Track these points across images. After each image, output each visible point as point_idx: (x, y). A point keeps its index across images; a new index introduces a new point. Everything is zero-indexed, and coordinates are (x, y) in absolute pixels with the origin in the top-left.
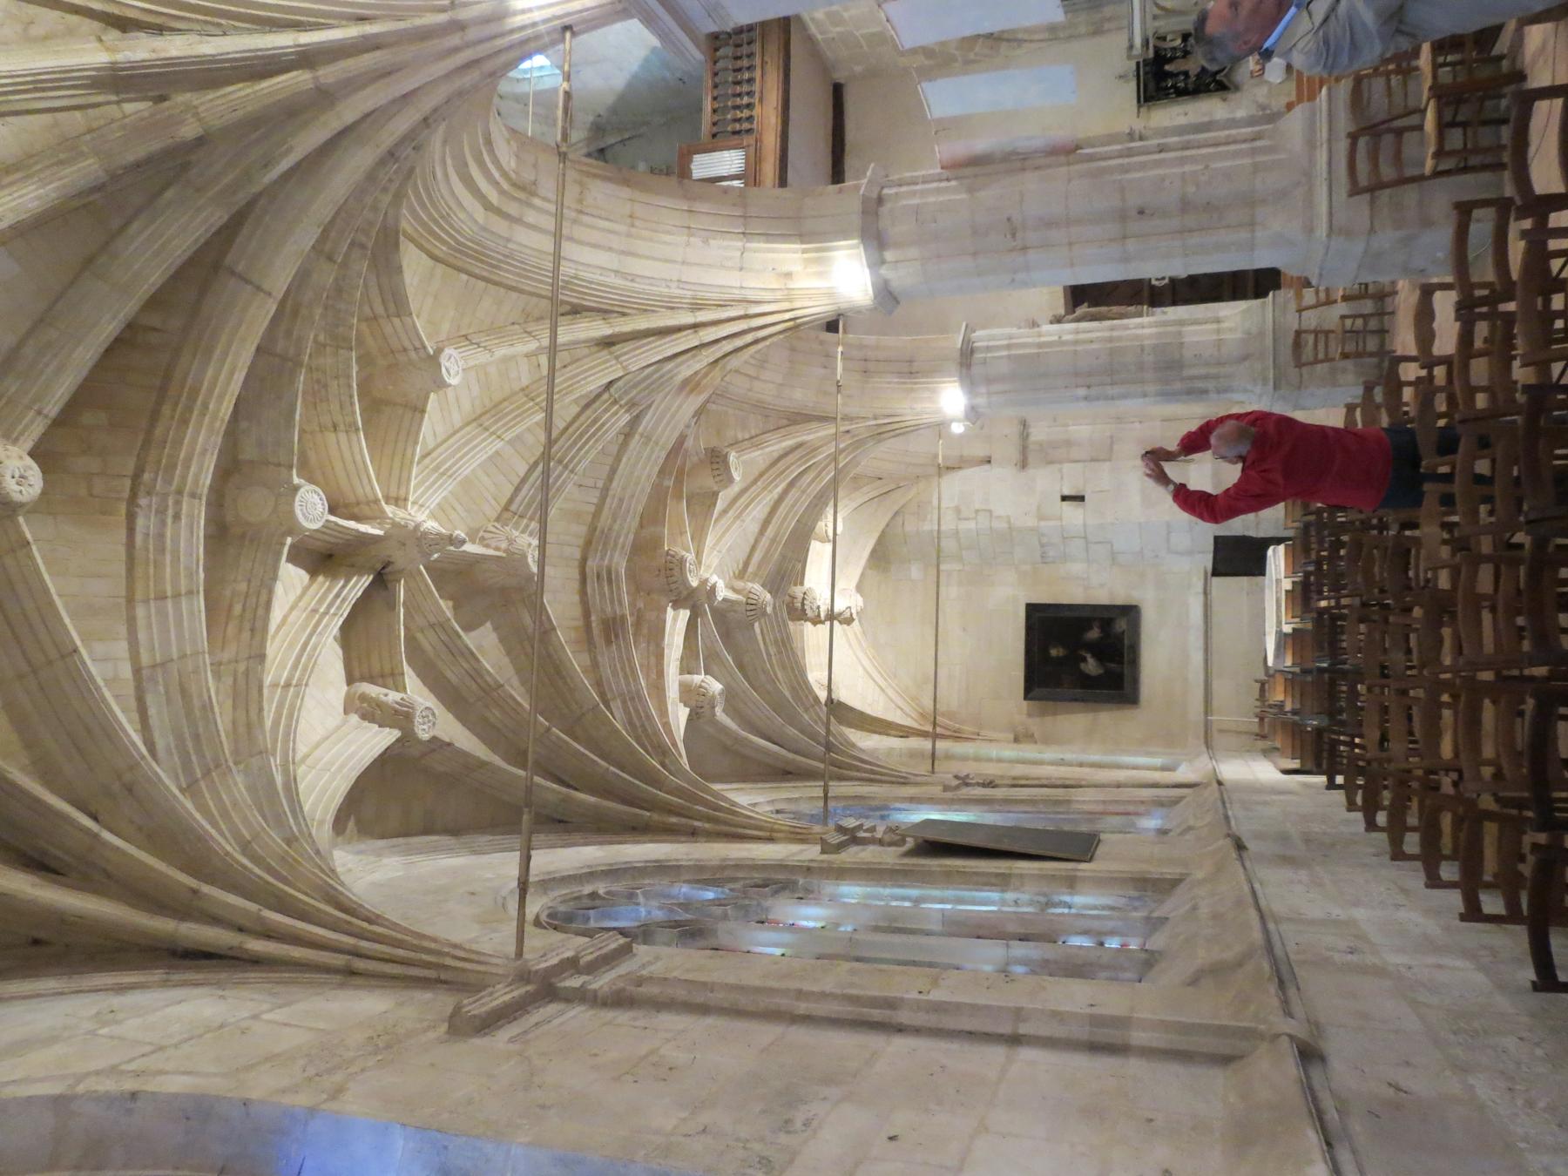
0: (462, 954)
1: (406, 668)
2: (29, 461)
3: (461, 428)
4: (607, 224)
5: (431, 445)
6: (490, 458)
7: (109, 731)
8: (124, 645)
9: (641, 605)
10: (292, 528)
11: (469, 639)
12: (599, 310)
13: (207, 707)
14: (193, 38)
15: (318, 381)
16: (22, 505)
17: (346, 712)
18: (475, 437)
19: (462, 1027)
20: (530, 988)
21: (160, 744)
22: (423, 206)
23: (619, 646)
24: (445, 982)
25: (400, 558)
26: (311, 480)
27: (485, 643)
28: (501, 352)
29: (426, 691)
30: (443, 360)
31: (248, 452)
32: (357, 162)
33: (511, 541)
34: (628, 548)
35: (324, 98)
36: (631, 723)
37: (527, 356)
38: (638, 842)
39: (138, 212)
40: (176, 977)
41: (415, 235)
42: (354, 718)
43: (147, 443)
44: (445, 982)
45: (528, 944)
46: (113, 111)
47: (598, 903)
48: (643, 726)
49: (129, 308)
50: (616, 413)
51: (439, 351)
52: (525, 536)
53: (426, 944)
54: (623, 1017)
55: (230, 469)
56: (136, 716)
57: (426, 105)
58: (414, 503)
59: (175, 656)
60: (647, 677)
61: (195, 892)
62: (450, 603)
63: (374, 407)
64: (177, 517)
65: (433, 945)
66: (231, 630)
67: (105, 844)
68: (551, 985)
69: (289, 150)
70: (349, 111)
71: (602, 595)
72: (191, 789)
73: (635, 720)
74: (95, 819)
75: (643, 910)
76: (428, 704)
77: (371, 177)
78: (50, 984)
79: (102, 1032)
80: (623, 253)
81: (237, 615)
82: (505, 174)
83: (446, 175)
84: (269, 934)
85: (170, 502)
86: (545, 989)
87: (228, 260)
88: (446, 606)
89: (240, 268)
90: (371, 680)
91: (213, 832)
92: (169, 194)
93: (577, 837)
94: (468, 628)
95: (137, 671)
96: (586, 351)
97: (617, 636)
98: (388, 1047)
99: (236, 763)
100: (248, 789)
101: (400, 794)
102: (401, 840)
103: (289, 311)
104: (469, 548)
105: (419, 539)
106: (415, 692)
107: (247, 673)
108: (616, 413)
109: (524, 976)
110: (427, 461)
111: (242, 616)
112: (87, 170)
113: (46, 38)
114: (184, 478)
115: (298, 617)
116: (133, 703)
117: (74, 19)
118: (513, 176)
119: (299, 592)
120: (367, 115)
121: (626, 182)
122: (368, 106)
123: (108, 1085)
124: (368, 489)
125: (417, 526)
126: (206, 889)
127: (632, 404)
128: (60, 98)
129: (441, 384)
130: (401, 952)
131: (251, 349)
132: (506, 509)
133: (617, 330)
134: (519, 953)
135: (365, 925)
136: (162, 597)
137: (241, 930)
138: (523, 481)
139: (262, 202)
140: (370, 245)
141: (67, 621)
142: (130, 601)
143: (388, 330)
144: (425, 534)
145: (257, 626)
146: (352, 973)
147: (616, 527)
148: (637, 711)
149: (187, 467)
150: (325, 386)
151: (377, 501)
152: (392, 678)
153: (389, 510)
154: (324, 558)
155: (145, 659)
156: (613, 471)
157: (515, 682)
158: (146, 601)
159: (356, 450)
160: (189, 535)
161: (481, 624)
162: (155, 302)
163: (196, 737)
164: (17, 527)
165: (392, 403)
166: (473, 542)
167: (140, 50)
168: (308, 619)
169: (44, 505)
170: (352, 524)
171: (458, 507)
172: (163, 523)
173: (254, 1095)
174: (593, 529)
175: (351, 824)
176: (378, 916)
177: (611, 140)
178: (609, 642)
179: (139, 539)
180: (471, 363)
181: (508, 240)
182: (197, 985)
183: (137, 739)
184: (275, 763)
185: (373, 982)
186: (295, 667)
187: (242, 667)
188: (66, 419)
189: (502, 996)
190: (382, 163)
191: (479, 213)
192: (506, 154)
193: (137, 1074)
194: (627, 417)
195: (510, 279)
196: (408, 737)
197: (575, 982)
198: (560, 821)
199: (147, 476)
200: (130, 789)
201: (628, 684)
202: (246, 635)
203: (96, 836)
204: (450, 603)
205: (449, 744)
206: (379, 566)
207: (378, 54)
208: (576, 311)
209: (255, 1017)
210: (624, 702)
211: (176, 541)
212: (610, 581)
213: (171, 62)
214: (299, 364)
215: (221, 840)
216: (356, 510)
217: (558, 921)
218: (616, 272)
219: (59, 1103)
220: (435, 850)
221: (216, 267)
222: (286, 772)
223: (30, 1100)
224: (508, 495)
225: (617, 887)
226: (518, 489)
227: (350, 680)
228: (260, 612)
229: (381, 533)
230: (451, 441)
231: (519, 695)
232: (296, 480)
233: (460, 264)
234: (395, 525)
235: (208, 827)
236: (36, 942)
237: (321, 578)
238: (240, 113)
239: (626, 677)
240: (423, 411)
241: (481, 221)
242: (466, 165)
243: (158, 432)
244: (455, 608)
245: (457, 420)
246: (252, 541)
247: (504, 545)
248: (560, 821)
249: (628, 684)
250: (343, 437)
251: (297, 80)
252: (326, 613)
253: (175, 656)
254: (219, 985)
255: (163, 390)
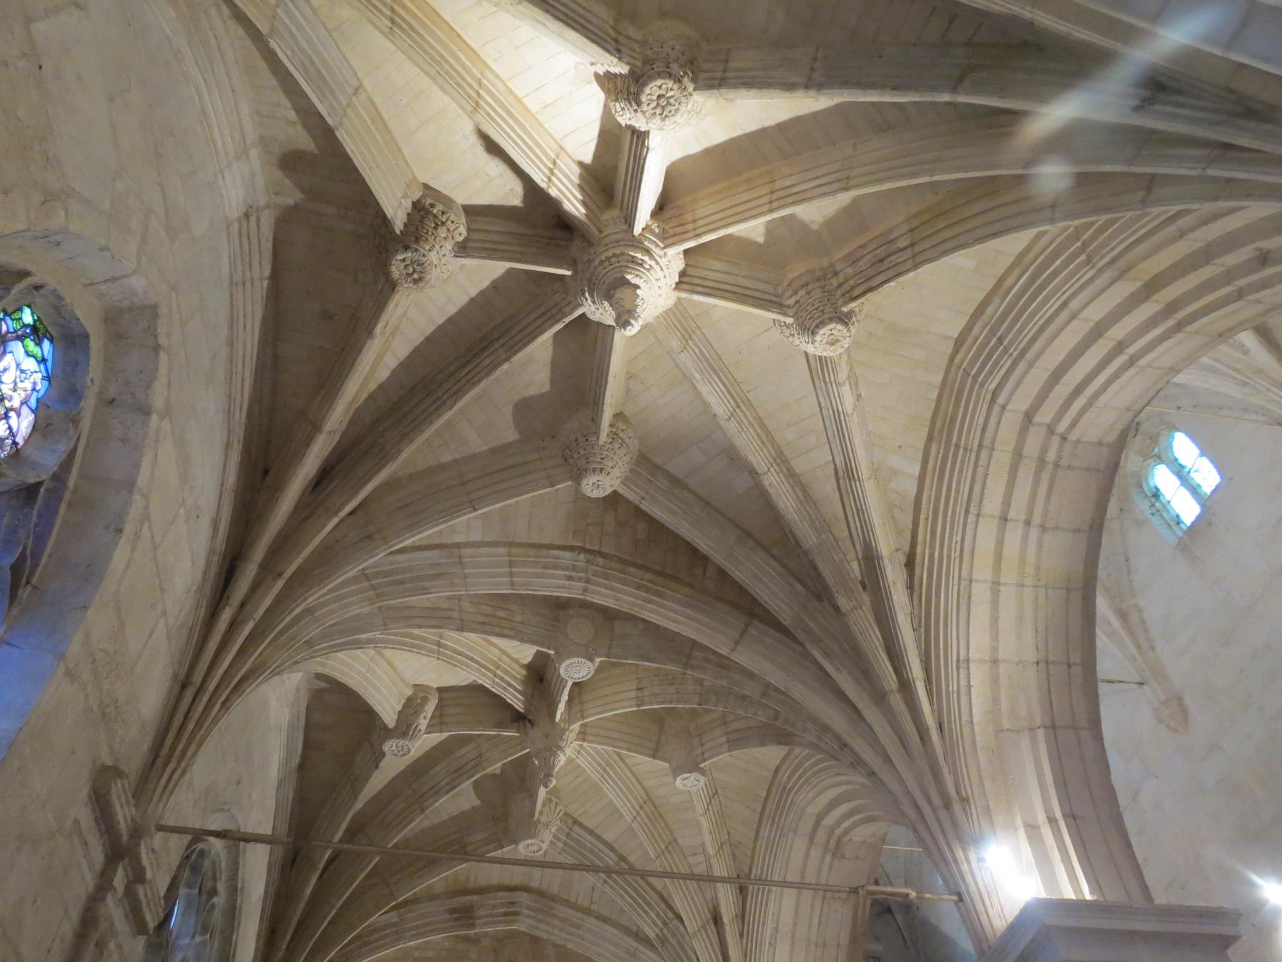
0: (176, 776)
1: (445, 735)
2: (609, 491)
3: (643, 787)
4: (816, 921)
5: (628, 761)
6: (618, 810)
7: (412, 527)
8: (478, 538)
9: (485, 942)
10: (561, 656)
11: (467, 785)
12: (744, 911)
13: (425, 591)
14: (908, 609)
15: (674, 679)
16: (579, 484)
17: (415, 686)
18: (635, 798)
19: (103, 777)
20: (125, 838)
21: (401, 557)
22: (813, 766)
23: (444, 921)
24: (154, 762)
25: (535, 733)
26: (599, 670)
27: (463, 799)
28: (704, 822)
29: (425, 749)
30: (694, 775)
31: (619, 627)
32: (838, 721)
33: (547, 825)
34: (537, 933)
35: (880, 698)
36: (373, 932)
37: (703, 845)
38: (259, 935)
39: (785, 566)
40: (215, 559)
41: (792, 756)
42: (409, 692)
43: (622, 561)
44: (154, 762)
45: (175, 837)
46: (851, 555)
47: (204, 897)
48: (369, 943)
49: (718, 558)
50: (656, 924)
51: (702, 772)
52: (551, 837)
53: (193, 747)
54: (68, 929)
55: (609, 616)
56: (424, 543)
57: (885, 776)
58: (581, 746)
59: (466, 571)
60: (417, 948)
61: (280, 575)
62: (498, 772)
63: (659, 719)
64: (570, 578)
65: (190, 753)
66: (485, 609)
67: (329, 519)
68: (122, 857)
69: (838, 670)
70: (872, 714)
71: (494, 907)
72: (364, 576)
73: (376, 936)
74: (351, 513)
75: (187, 941)
76: (413, 751)
77: (826, 729)
78: (232, 479)
79: (182, 511)
80: (793, 936)
81: (496, 615)
82: (846, 832)
83: (839, 784)
84: (234, 625)
85: (582, 575)
86: (120, 852)
87: (756, 622)
88: (496, 768)
89: (751, 630)
90: (440, 707)
91: (325, 590)
92: (799, 587)
93: (276, 876)
94: (476, 785)
95: (458, 546)
96: (708, 898)
97: (456, 919)
98: (104, 715)
99: (379, 608)
100: (358, 615)
101: (341, 726)
102: (303, 722)
103: (724, 664)
104: (542, 793)
105: (552, 748)
106: (424, 741)
107: (450, 618)
108: (656, 924)
109: (137, 833)
110: (616, 757)
111: (495, 616)
112: (809, 538)
113: (893, 518)
114: (598, 585)
115: (494, 654)
116: (437, 541)
117: (908, 534)
118: (846, 839)
119: (515, 656)
120: (871, 729)
121: (854, 940)
122: (877, 729)
123: (135, 511)
124: (593, 711)
125: (561, 749)
126: (280, 584)
127: (663, 940)
128: (855, 524)
129: (676, 772)
130: (191, 726)
131: (692, 634)
132: (575, 822)
133: (727, 928)
134: (161, 828)
135: (223, 698)
136: (511, 566)
137: (243, 605)
138: (599, 838)
139: (800, 649)
140: (777, 724)
141: (497, 506)
142: (511, 544)
143: (718, 732)
144: (555, 755)
145: (485, 627)
146: (184, 686)
147: (556, 922)
148: (387, 936)
149: (606, 587)
150: (672, 684)
151: (583, 718)
152: (438, 722)
153: (576, 727)
154: (539, 677)
155: (469, 551)
156: (605, 920)
157: (426, 824)
158: (509, 555)
159: (627, 703)
160: (555, 585)
161: (479, 797)
162: (723, 574)
163: (402, 582)
164: (563, 481)
165: (659, 732)
166: (547, 793)
167: (894, 576)
168: (492, 662)
169: (580, 497)
170: (565, 697)
171: (578, 781)
172: (564, 570)
173: (90, 613)
174: (553, 899)
175: (323, 685)
176: (228, 708)
177: (899, 918)
178: (452, 911)
179: (556, 552)
180: (695, 798)
181: (795, 832)
182: (205, 573)
183: (407, 543)
184: (377, 635)
185: (172, 702)
186: (454, 651)
187: (455, 615)
188: (638, 512)
189: (123, 814)
190: (838, 738)
191: (813, 809)
192: (864, 833)
193: (137, 534)
194: (652, 935)
195: (765, 832)
196: (388, 733)
197: (119, 881)
198: (294, 860)
199: (600, 560)
200: (369, 537)
201: (410, 929)
202: (480, 618)
203: (336, 513)
204: (498, 772)
205: (377, 767)
206: (530, 717)
207: (918, 739)
208: (742, 890)
209: (164, 614)
210: (395, 925)
211: (553, 577)
212: (505, 914)
213: (889, 594)
214: (686, 666)
215: (317, 595)
216: (576, 701)
217: (192, 862)
218: (776, 929)
219: (130, 484)
220: (289, 752)
221: (752, 615)
222: (368, 641)
223: (137, 466)
224: (587, 824)
225: (217, 918)
226: (591, 832)
227: (441, 690)
228: (497, 630)
229: (558, 719)
230: (632, 777)
231: (418, 824)
232: (598, 660)
233: (774, 789)
234: (564, 731)
235: (329, 587)
236: (266, 472)
237: (524, 672)
238: (860, 638)
239: (417, 927)
240: (654, 757)
241: (809, 810)
242: (850, 800)
243: (632, 570)
244: (494, 777)
245: (649, 783)
246: (553, 626)
247: (544, 819)
248: (294, 860)
249: (410, 929)
250: (633, 694)
251: (889, 680)
252: (495, 675)
253: (466, 571)
254: (200, 589)
255: (661, 574)
